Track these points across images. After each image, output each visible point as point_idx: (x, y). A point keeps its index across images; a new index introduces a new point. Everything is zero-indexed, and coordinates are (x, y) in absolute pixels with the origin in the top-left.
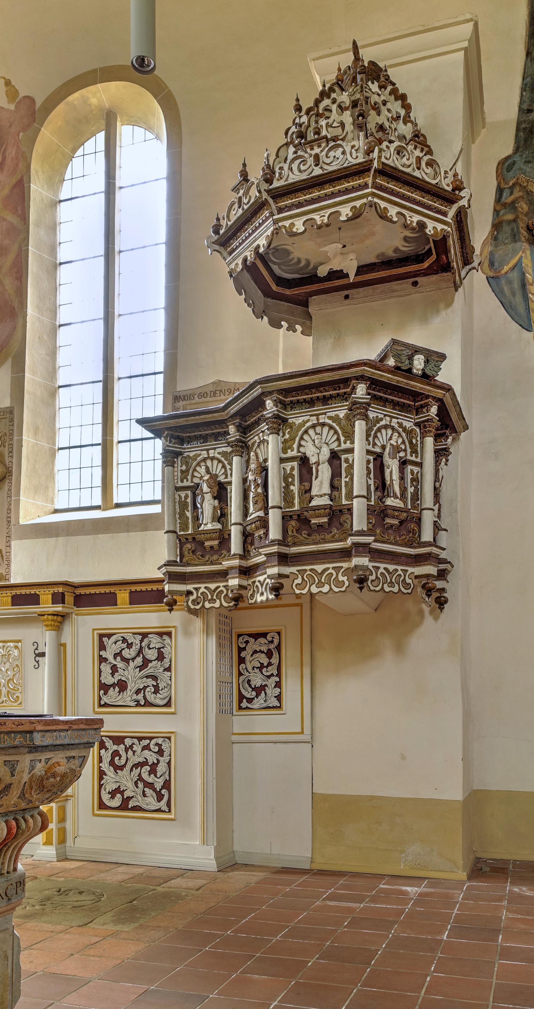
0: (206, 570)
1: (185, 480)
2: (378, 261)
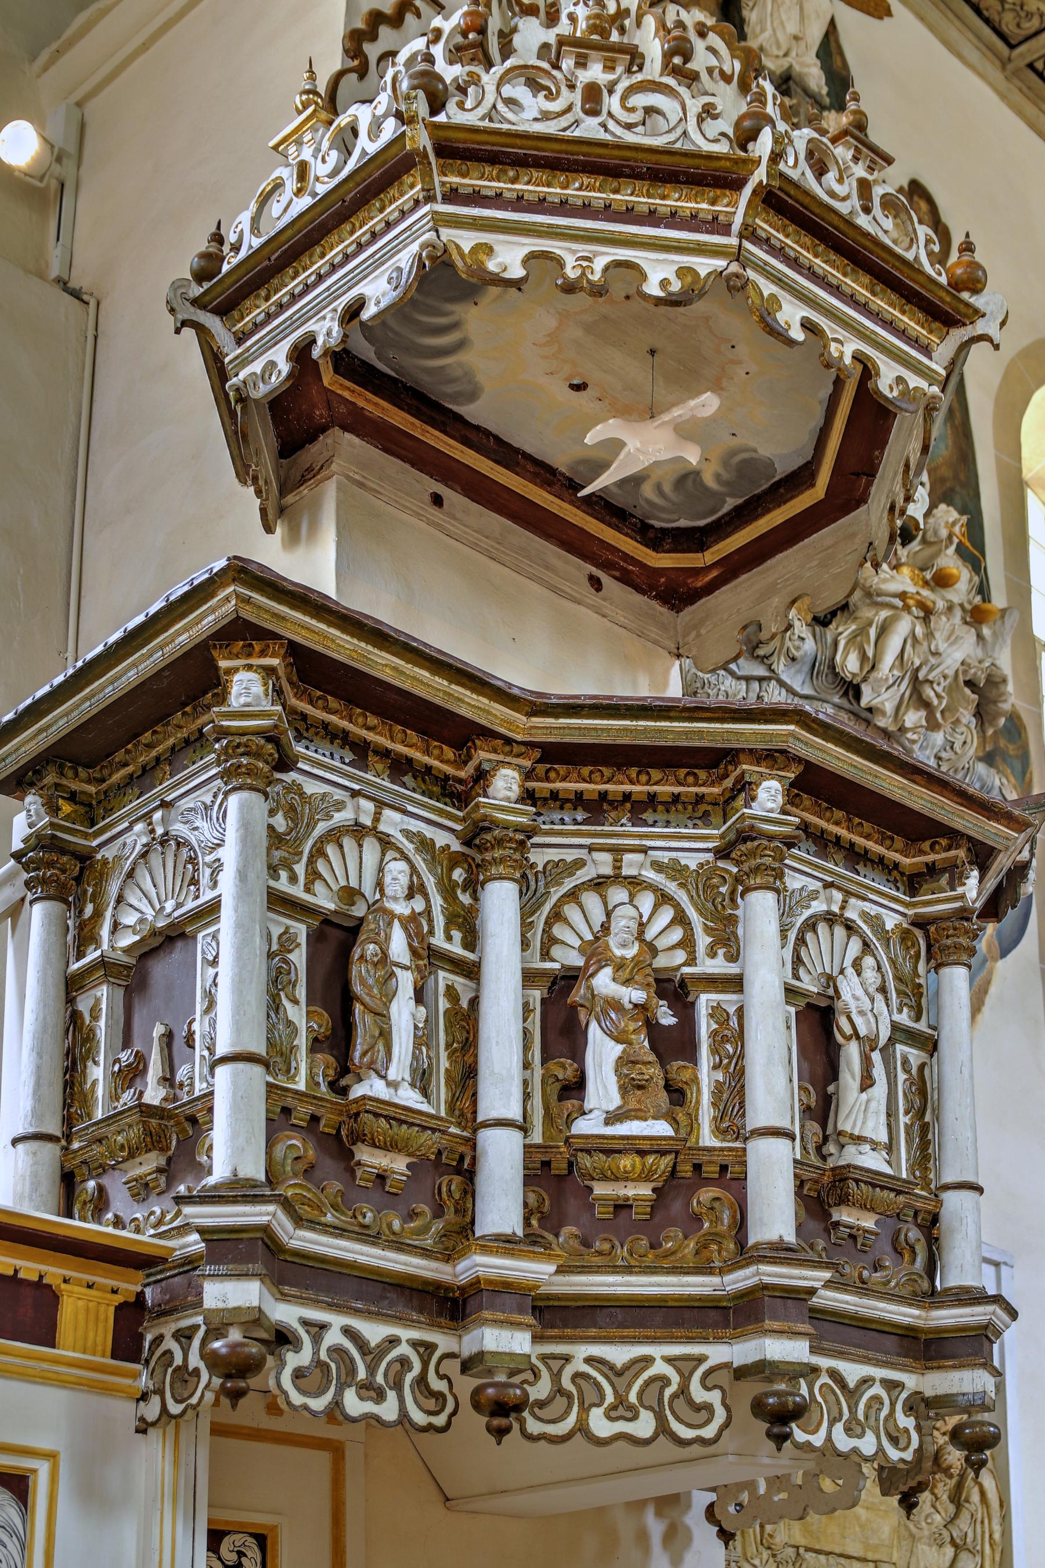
0: (362, 1259)
1: (284, 875)
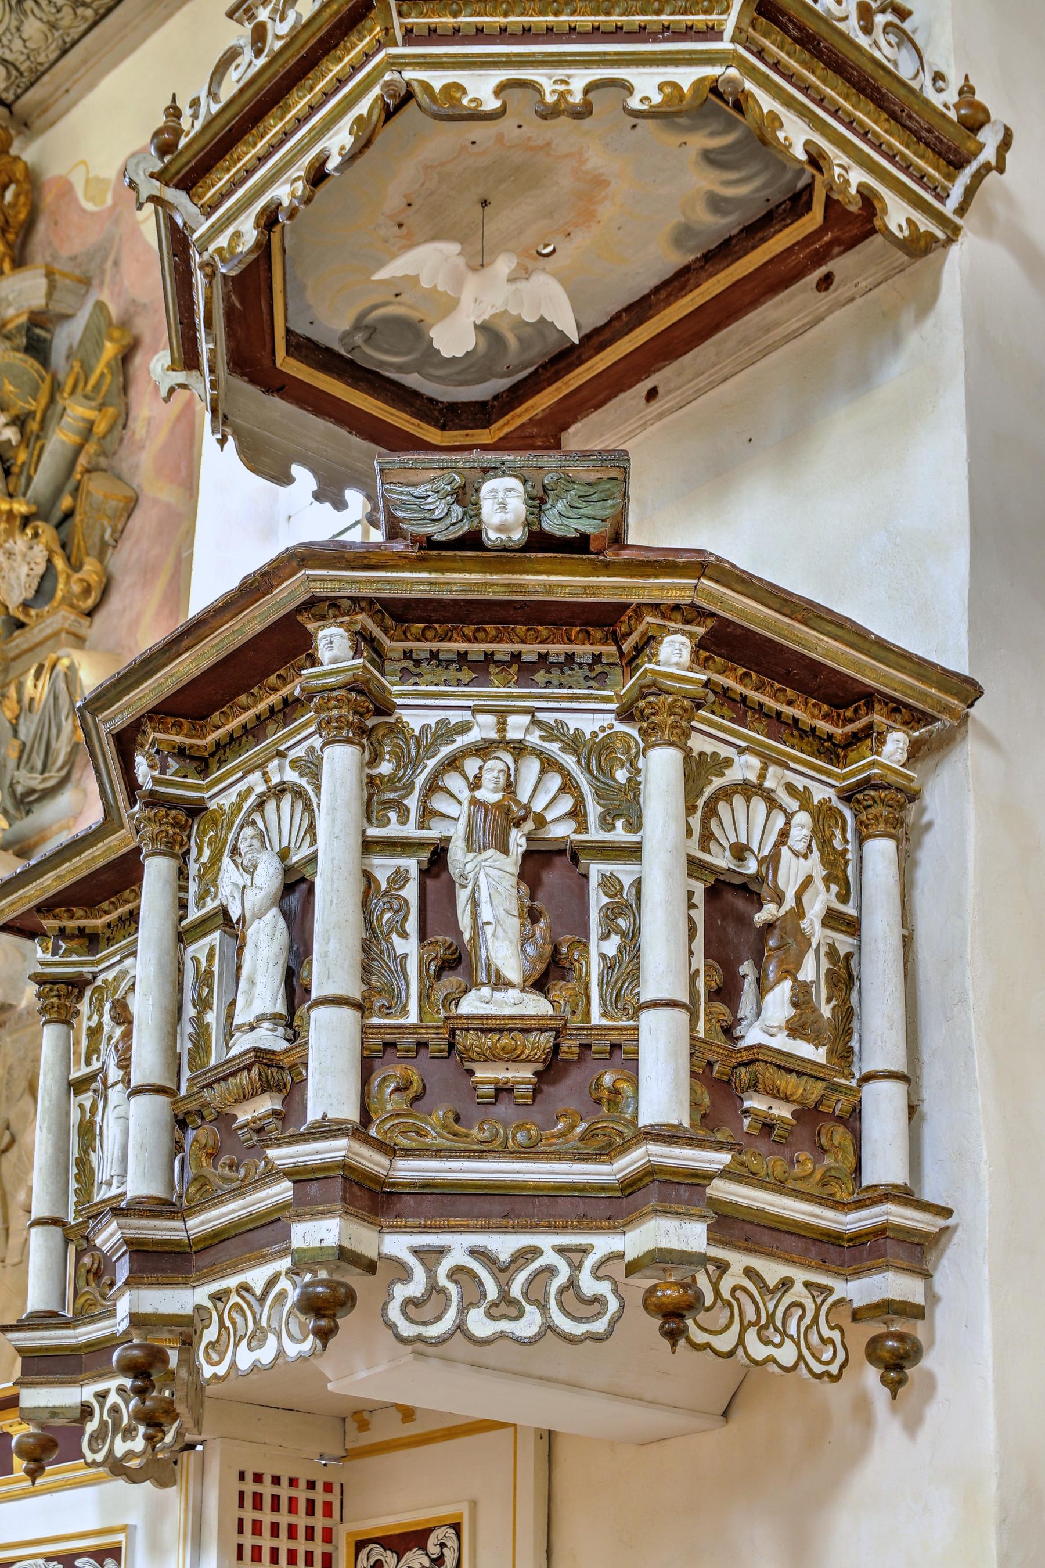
2: (691, 258)
